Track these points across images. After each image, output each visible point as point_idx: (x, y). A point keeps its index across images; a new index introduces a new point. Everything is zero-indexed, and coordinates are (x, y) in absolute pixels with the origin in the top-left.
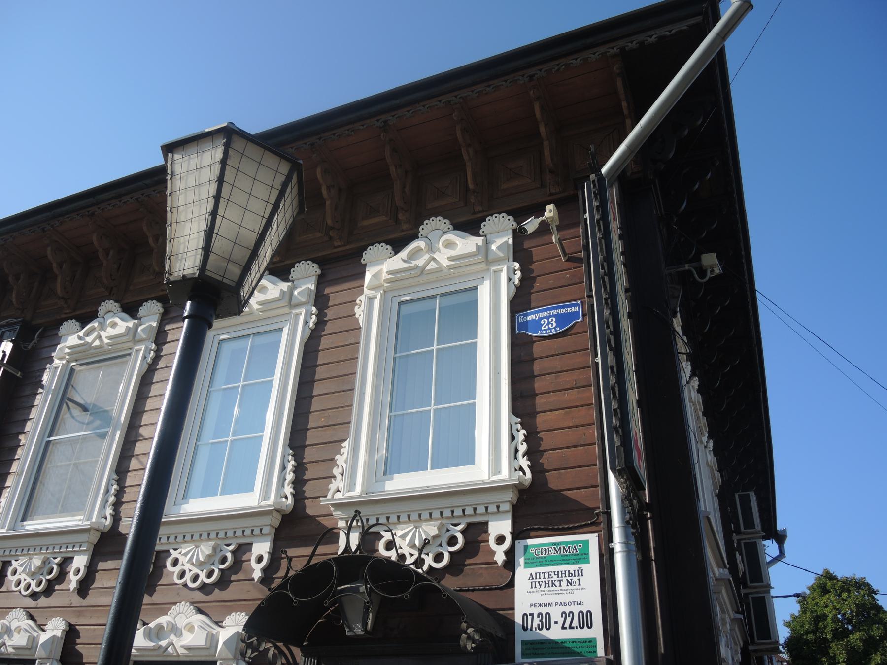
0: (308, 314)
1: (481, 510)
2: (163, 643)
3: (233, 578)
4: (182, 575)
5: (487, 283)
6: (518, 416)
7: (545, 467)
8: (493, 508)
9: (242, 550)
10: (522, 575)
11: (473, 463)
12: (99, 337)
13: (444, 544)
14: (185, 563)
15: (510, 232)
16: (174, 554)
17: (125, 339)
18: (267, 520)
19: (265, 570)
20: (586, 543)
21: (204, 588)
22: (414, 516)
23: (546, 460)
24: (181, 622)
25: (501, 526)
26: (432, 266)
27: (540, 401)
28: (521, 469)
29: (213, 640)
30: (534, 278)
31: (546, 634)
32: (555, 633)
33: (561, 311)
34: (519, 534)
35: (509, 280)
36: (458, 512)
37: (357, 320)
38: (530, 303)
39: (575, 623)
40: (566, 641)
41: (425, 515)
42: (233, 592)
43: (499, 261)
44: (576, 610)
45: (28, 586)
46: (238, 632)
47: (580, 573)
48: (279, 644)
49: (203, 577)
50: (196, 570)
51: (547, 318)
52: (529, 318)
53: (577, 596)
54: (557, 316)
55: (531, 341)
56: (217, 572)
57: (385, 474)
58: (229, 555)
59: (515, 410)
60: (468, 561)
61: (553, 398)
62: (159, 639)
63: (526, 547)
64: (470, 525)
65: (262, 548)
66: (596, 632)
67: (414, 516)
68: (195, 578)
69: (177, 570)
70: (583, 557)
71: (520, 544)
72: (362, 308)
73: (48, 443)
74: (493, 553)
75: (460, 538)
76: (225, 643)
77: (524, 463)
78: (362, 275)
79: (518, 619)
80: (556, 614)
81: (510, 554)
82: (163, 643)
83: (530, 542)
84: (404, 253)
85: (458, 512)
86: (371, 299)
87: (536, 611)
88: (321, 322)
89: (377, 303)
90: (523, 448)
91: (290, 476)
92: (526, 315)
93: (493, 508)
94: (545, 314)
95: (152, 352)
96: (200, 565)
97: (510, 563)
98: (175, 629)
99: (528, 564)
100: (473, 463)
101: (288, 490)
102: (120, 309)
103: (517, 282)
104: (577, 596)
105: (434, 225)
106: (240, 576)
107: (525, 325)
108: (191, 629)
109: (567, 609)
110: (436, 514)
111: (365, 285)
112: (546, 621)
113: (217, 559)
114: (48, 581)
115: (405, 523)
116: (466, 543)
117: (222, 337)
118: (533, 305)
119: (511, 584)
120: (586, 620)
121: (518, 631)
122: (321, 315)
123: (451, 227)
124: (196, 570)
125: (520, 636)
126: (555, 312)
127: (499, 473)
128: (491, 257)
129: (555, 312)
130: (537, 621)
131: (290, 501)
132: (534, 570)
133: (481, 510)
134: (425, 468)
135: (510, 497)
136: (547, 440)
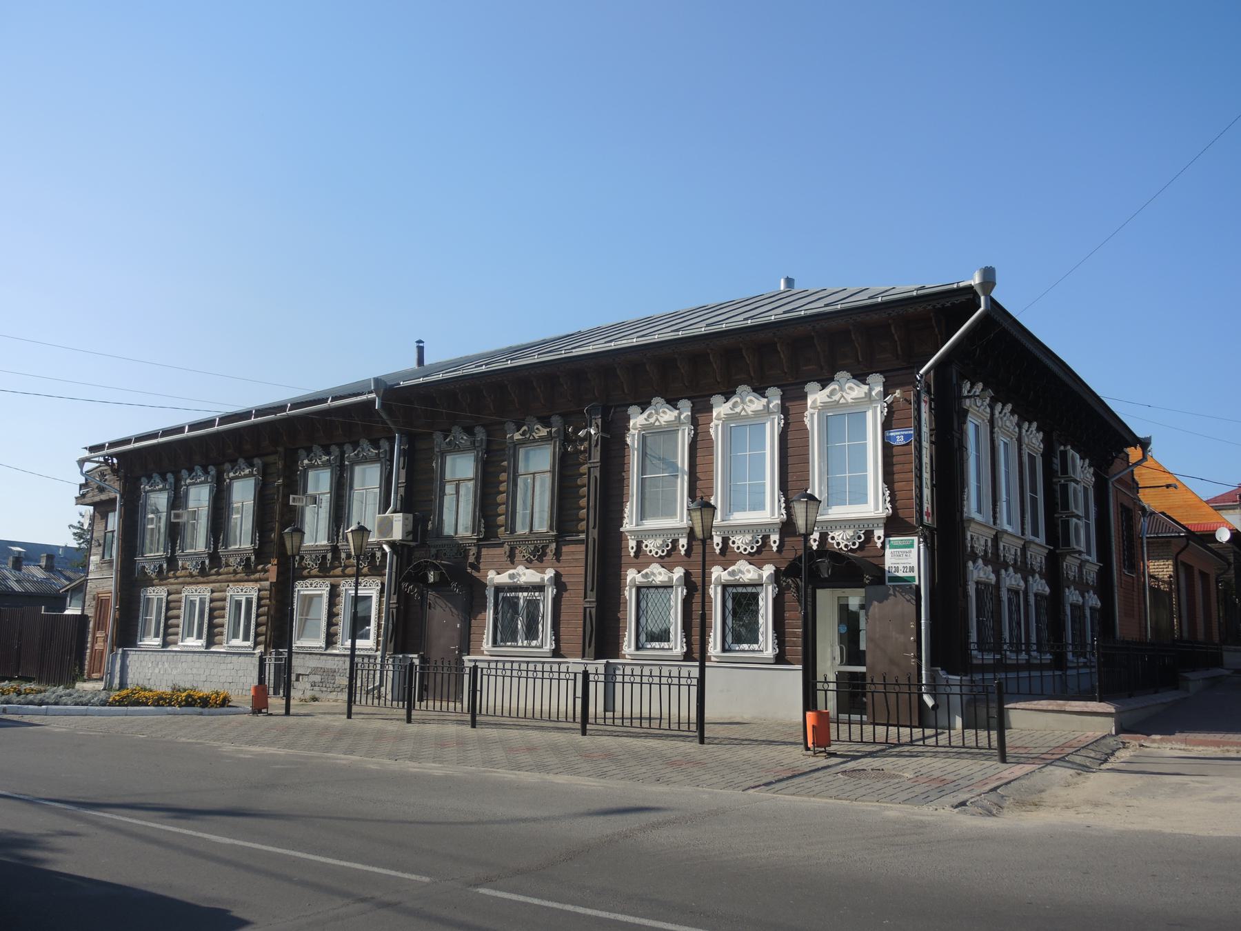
0: (780, 419)
1: (767, 530)
2: (737, 577)
3: (763, 549)
4: (738, 548)
5: (871, 411)
6: (886, 484)
7: (898, 507)
8: (876, 525)
9: (675, 542)
10: (888, 552)
11: (867, 503)
12: (657, 419)
13: (856, 538)
14: (651, 547)
15: (882, 383)
16: (732, 539)
17: (763, 412)
18: (777, 526)
19: (635, 552)
20: (913, 540)
21: (661, 557)
22: (843, 527)
23: (898, 504)
24: (655, 571)
25: (879, 532)
26: (743, 413)
27: (896, 476)
28: (887, 508)
29: (543, 579)
30: (894, 412)
31: (897, 574)
32: (900, 574)
33: (906, 433)
34: (886, 535)
35: (689, 434)
36: (861, 526)
37: (806, 425)
38: (891, 425)
39: (908, 571)
40: (904, 577)
41: (847, 527)
42: (764, 555)
43: (773, 413)
44: (908, 566)
45: (657, 553)
46: (771, 573)
47: (910, 552)
48: (273, 588)
49: (660, 552)
50: (656, 550)
51: (900, 435)
52: (892, 434)
53: (909, 560)
54: (904, 435)
55: (892, 446)
56: (665, 551)
57: (730, 512)
58: (760, 540)
59: (885, 481)
60: (867, 546)
61: (902, 476)
62: (514, 579)
63: (890, 541)
64: (673, 540)
65: (775, 537)
66: (915, 574)
67: (843, 527)
68: (745, 550)
69: (735, 546)
70: (912, 546)
71: (887, 539)
72: (808, 418)
73: (642, 478)
74: (680, 551)
75: (863, 536)
76: (767, 578)
77: (889, 506)
78: (711, 411)
79: (887, 568)
80: (901, 567)
81: (883, 543)
82: (515, 580)
83: (891, 539)
84: (730, 404)
85: (861, 526)
86: (812, 415)
87: (893, 566)
88: (786, 424)
89: (816, 417)
90: (888, 499)
91: (783, 505)
92: (890, 432)
93: (876, 525)
94: (898, 433)
95: (886, 409)
96: (658, 547)
97: (883, 547)
98: (740, 571)
99: (890, 548)
100: (867, 503)
101: (784, 511)
102: (665, 402)
103: (885, 414)
104: (909, 560)
105: (842, 376)
106: (767, 548)
107: (177, 516)
108: (660, 574)
109: (905, 565)
110: (852, 526)
111: (809, 407)
112: (897, 569)
113: (754, 541)
114: (667, 550)
115: (839, 529)
116: (865, 538)
117: (732, 425)
118: (894, 427)
119: (884, 555)
120: (912, 569)
121: (887, 573)
122: (695, 430)
123: (851, 377)
124: (656, 550)
125: (887, 575)
126: (903, 433)
127: (878, 510)
128: (872, 399)
129: (903, 433)
130: (894, 569)
131: (785, 516)
132: (893, 550)
133: (767, 530)
134: (746, 511)
135: (882, 521)
136: (899, 495)
